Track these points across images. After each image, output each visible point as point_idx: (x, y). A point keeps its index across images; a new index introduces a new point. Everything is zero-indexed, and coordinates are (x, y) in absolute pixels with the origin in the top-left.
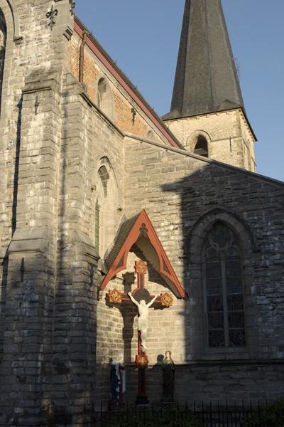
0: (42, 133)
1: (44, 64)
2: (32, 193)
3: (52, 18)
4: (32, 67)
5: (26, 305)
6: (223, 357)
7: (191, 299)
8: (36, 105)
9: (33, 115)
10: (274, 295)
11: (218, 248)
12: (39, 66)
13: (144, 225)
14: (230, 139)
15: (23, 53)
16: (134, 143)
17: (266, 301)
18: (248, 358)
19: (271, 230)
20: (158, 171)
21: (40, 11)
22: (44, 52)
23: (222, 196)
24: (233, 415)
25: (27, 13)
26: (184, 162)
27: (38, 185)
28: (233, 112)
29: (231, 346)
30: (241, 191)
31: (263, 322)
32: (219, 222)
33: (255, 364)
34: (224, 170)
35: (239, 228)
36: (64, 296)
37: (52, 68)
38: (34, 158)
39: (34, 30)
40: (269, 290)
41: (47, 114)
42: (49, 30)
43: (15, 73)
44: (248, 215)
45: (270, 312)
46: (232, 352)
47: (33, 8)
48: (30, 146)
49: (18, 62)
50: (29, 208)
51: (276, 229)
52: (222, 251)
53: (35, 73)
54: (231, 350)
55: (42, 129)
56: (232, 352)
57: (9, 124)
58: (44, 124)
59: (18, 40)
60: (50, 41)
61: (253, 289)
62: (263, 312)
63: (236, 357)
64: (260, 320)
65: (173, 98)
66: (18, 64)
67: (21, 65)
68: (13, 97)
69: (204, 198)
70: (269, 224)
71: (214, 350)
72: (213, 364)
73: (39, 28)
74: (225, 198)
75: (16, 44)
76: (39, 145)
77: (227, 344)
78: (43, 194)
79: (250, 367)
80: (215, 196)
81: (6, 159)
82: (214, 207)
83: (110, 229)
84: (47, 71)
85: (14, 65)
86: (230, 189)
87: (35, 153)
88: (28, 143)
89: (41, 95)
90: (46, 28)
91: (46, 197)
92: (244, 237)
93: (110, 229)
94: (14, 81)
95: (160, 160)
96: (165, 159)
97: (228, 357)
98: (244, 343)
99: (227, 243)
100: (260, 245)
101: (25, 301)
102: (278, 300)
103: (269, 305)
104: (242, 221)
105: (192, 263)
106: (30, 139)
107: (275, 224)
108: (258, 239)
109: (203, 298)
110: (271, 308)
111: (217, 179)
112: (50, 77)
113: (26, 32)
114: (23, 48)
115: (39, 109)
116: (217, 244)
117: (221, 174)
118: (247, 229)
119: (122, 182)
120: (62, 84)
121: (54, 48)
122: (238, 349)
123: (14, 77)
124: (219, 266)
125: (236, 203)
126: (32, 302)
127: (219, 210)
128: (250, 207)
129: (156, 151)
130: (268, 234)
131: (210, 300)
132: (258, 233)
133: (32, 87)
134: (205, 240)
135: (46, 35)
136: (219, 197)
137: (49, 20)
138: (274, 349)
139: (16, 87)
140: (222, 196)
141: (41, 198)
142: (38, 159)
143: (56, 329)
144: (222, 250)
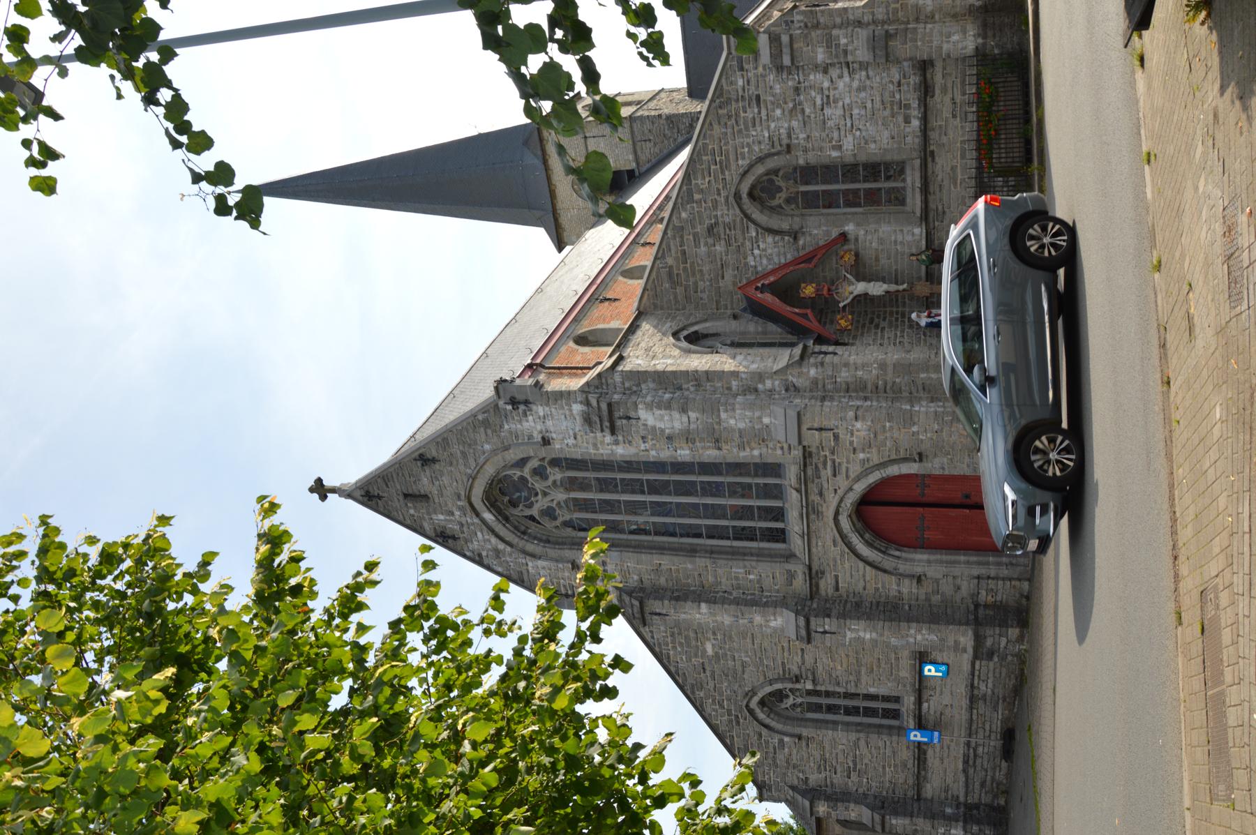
0: (663, 412)
1: (575, 412)
2: (732, 422)
3: (519, 403)
4: (578, 424)
5: (858, 425)
6: (918, 190)
7: (846, 228)
8: (629, 418)
9: (640, 423)
10: (842, 128)
11: (783, 195)
12: (577, 418)
13: (757, 288)
14: (586, 137)
15: (561, 437)
16: (649, 299)
17: (850, 138)
18: (919, 161)
19: (762, 131)
20: (685, 269)
21: (510, 418)
22: (561, 412)
23: (718, 190)
24: (986, 180)
25: (511, 432)
26: (674, 237)
27: (723, 415)
28: (583, 160)
29: (904, 180)
30: (713, 167)
31: (875, 142)
32: (751, 195)
33: (927, 155)
34: (685, 188)
35: (760, 170)
36: (688, 431)
37: (581, 403)
38: (692, 420)
39: (533, 424)
40: (836, 135)
41: (640, 406)
42: (534, 407)
43: (585, 444)
44: (743, 158)
45: (864, 134)
46: (912, 178)
47: (506, 427)
48: (677, 425)
49: (571, 441)
50: (749, 424)
51: (761, 125)
52: (787, 189)
53: (587, 420)
54: (909, 180)
55: (658, 412)
56: (912, 178)
57: (647, 450)
58: (652, 409)
59: (546, 441)
60: (547, 405)
61: (835, 154)
62: (863, 142)
63: (917, 175)
64: (873, 146)
65: (351, 165)
66: (574, 442)
67: (575, 438)
68: (614, 447)
69: (719, 213)
70: (754, 133)
71: (908, 200)
72: (926, 202)
73: (530, 418)
74: (721, 187)
75: (549, 444)
76: (676, 415)
77: (902, 185)
78: (734, 410)
79: (929, 159)
80: (718, 199)
81: (688, 452)
82: (731, 199)
83: (760, 329)
84: (585, 408)
85: (575, 446)
86: (709, 182)
87: (685, 419)
88: (673, 428)
89: (617, 414)
90: (530, 410)
91: (737, 406)
92: (771, 164)
93: (760, 329)
94: (595, 445)
95: (671, 267)
96: (670, 261)
97: (918, 184)
98: (903, 162)
99: (777, 183)
100: (781, 145)
101: (853, 426)
102: (849, 124)
103: (854, 135)
104: (751, 166)
105: (802, 227)
106: (668, 425)
107: (754, 125)
108: (773, 146)
109: (845, 214)
110: (858, 133)
111: (697, 197)
112: (594, 403)
113: (535, 434)
114: (554, 436)
115: (632, 414)
116: (778, 195)
117: (690, 193)
118: (760, 160)
119: (699, 315)
120: (600, 390)
121: (556, 400)
122: (908, 171)
123: (591, 446)
124: (805, 194)
125: (727, 173)
126: (856, 418)
127: (735, 194)
128: (732, 157)
129: (658, 272)
130: (767, 135)
131: (849, 204)
132: (765, 147)
133: (607, 424)
134: (772, 209)
135: (541, 410)
136: (719, 194)
137: (522, 407)
138: (908, 130)
139: (602, 443)
140: (718, 190)
141: (738, 412)
142: (693, 415)
143: (885, 392)
144: (785, 190)
